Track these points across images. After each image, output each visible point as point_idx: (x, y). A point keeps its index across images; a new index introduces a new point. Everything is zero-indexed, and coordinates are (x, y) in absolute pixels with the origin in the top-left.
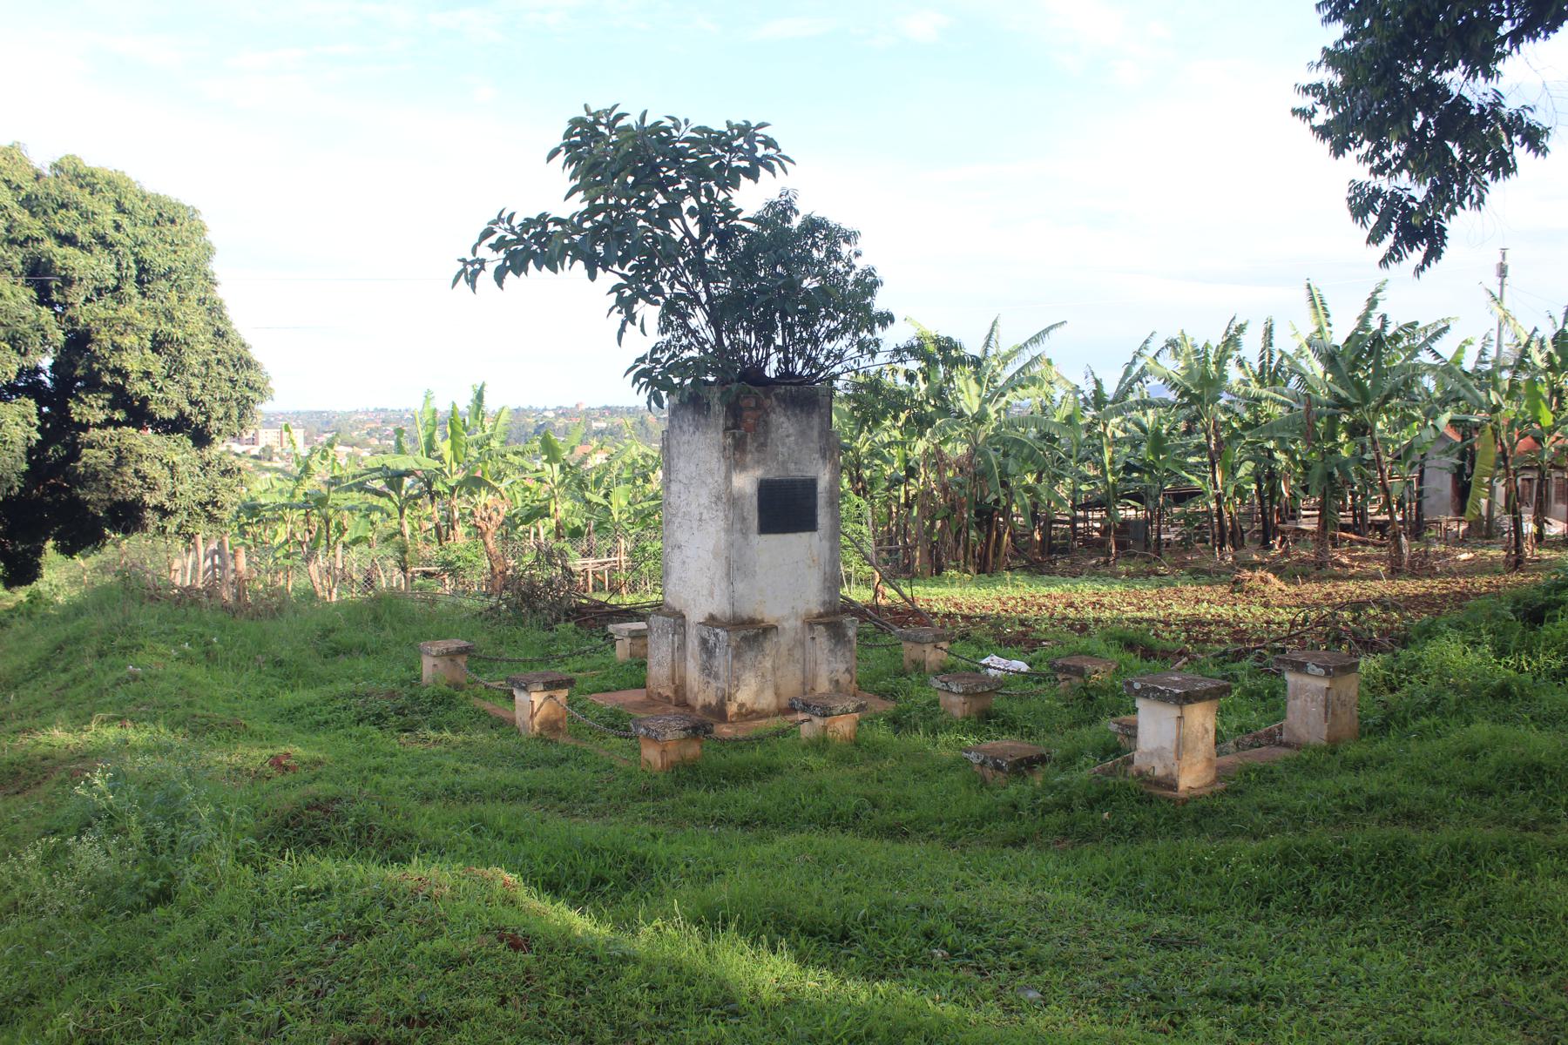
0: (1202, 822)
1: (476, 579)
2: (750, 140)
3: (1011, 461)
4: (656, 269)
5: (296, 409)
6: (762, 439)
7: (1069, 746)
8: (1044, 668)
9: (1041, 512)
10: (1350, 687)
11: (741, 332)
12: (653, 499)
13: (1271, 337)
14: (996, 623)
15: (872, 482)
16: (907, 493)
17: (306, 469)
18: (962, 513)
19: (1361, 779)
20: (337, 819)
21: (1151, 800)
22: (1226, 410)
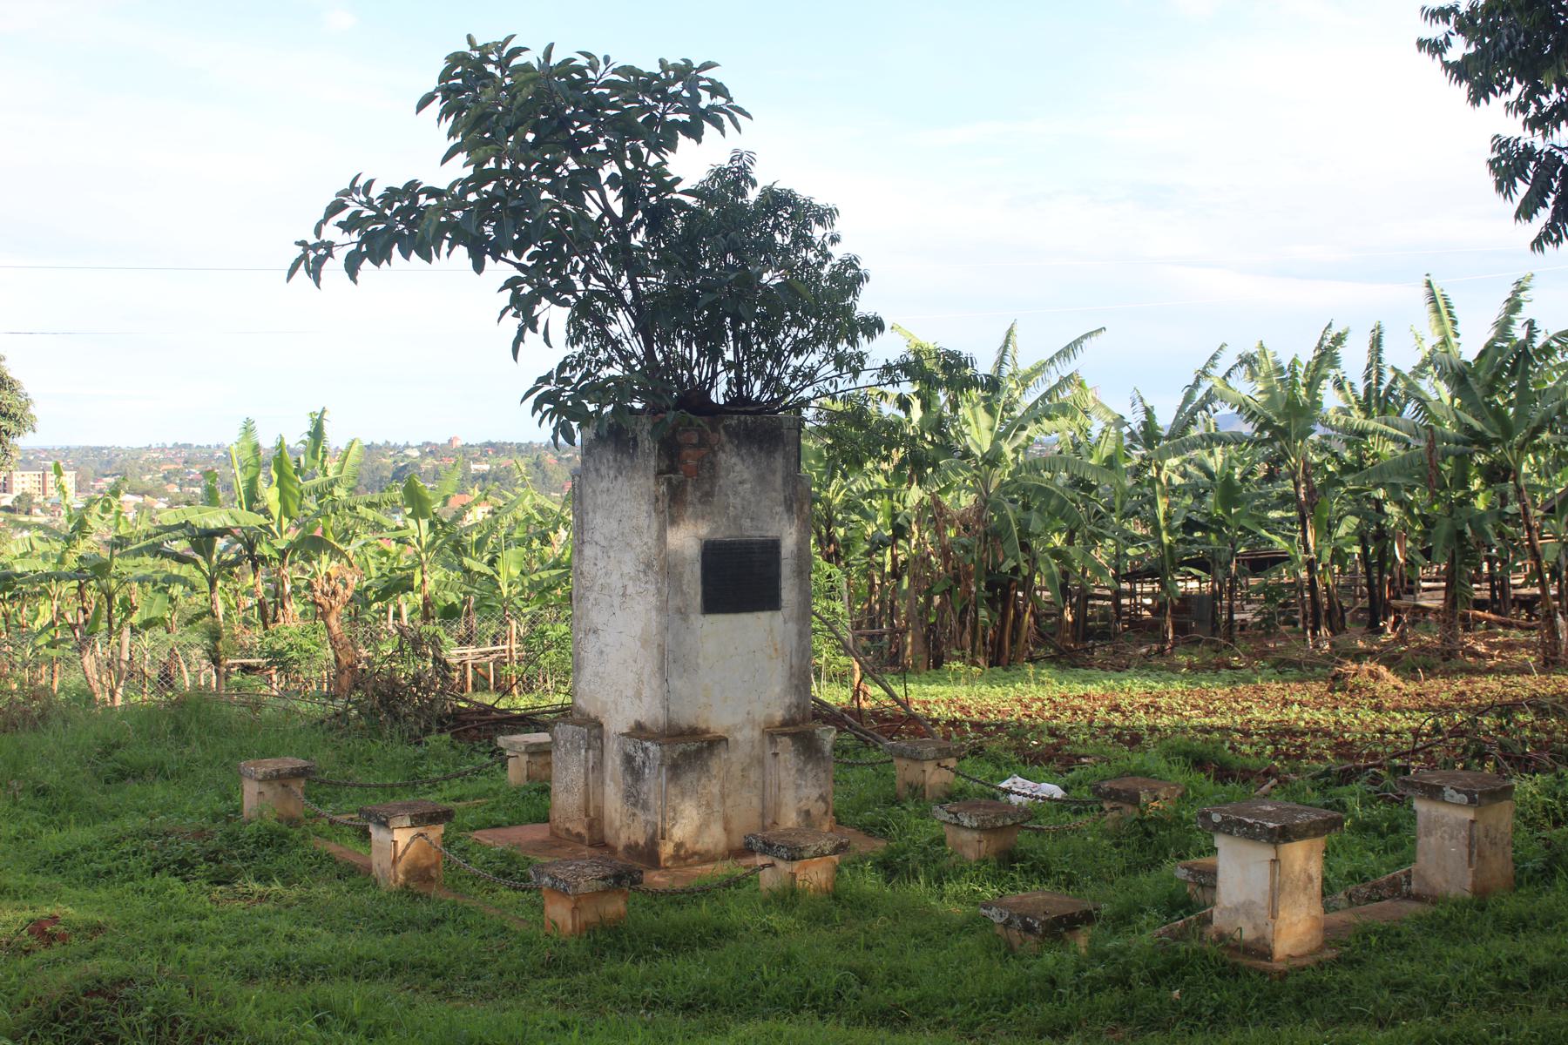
0: (1308, 1004)
1: (318, 671)
2: (692, 85)
3: (1034, 516)
4: (566, 259)
5: (64, 444)
6: (707, 487)
7: (1121, 899)
8: (1085, 793)
9: (1074, 584)
10: (1502, 817)
11: (678, 343)
12: (554, 567)
13: (1379, 350)
14: (1017, 732)
15: (848, 543)
16: (894, 558)
17: (81, 527)
18: (968, 586)
19: (1521, 945)
20: (128, 1010)
21: (1235, 972)
22: (1322, 448)
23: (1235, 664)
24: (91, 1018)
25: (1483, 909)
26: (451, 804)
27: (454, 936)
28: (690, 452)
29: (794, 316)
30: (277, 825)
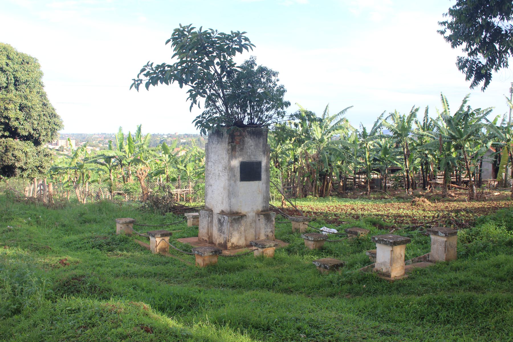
0: (399, 289)
1: (137, 196)
2: (239, 38)
6: (242, 147)
7: (351, 260)
8: (343, 232)
9: (343, 175)
10: (454, 240)
11: (235, 108)
12: (202, 168)
13: (427, 113)
15: (282, 163)
16: (294, 167)
17: (76, 155)
20: (83, 283)
23: (386, 197)
24: (74, 285)
25: (448, 265)
26: (172, 231)
27: (172, 267)
28: (237, 137)
29: (266, 101)
30: (125, 236)
